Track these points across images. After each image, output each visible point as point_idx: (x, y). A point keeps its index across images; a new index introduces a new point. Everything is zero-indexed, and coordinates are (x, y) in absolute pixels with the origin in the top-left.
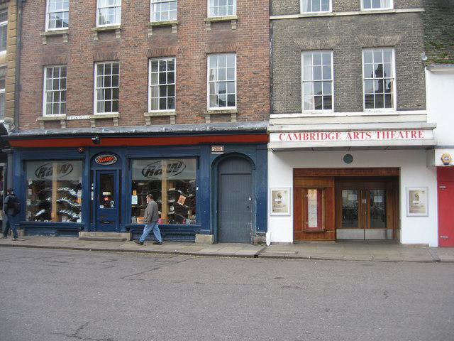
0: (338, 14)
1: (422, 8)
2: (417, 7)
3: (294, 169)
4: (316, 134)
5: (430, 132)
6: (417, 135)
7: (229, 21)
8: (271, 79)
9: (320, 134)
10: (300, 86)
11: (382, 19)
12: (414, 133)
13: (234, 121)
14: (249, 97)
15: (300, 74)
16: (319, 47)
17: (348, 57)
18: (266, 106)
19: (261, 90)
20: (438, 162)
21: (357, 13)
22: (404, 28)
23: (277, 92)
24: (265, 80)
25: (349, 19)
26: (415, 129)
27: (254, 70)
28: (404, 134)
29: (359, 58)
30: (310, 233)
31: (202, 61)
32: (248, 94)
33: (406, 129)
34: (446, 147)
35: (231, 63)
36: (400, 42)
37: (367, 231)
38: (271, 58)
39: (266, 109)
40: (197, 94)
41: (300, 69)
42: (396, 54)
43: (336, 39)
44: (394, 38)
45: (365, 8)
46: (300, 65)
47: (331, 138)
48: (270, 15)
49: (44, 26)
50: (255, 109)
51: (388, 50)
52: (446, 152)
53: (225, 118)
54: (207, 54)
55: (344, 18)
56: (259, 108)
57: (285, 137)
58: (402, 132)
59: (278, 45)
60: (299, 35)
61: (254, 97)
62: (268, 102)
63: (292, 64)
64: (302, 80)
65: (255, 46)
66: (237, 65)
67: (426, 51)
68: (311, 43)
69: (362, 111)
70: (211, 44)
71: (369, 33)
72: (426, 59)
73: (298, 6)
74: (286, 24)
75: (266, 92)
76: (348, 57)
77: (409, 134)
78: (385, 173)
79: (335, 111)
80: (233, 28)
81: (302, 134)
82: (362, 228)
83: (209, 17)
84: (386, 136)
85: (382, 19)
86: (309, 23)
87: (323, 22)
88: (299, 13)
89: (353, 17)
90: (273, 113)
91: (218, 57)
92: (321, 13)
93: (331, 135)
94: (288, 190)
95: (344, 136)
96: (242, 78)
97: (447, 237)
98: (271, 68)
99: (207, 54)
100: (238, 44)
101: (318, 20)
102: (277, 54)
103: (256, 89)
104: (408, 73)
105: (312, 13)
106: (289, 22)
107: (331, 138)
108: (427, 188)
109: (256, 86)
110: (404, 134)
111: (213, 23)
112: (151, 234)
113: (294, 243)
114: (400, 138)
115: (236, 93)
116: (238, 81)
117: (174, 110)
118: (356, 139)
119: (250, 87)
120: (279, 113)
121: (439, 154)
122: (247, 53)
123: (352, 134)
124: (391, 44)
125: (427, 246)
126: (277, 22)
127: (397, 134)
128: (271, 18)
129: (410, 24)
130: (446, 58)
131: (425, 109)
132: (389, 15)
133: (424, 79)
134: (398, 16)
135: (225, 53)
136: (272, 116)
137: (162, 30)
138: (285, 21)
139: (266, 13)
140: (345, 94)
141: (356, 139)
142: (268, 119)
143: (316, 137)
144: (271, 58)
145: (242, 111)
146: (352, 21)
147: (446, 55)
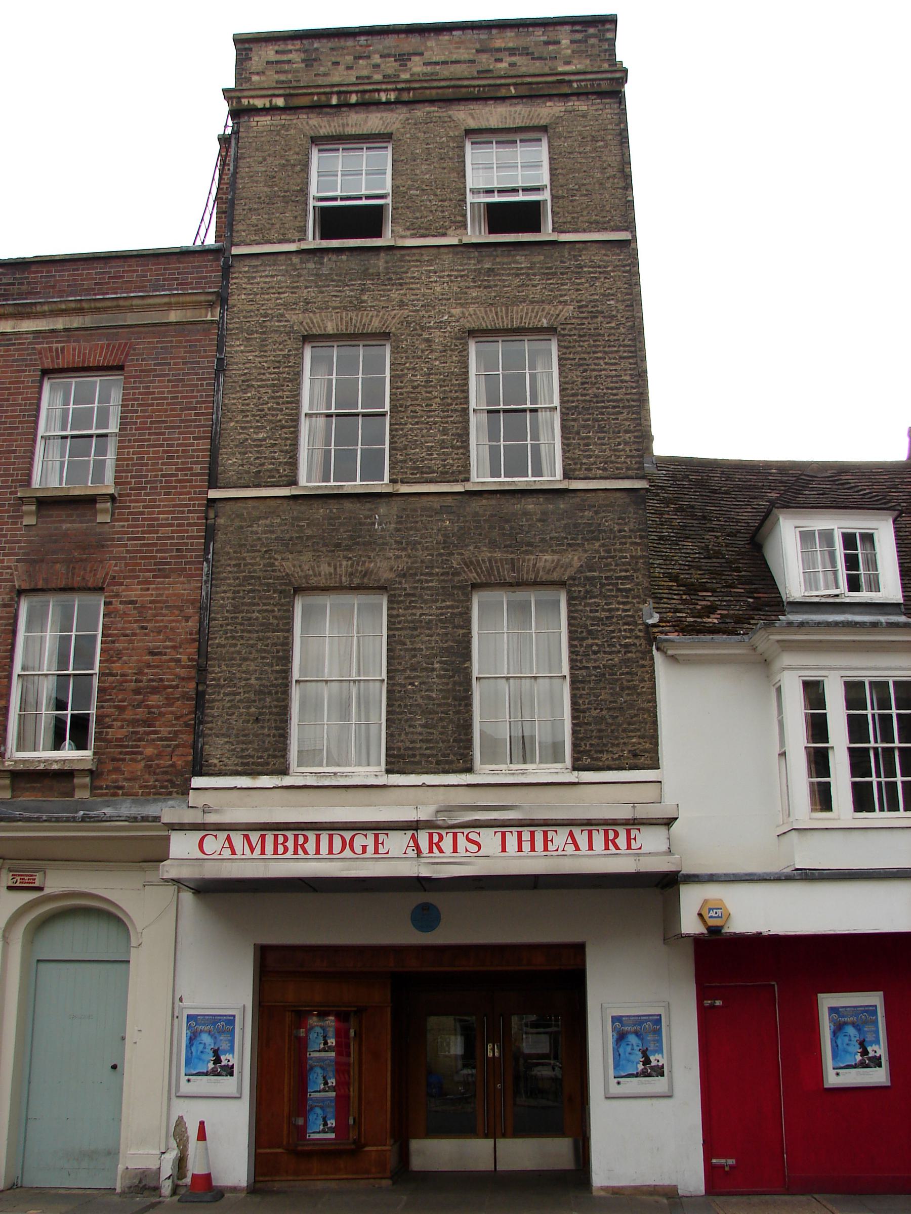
0: (404, 489)
2: (628, 478)
4: (311, 835)
5: (661, 831)
6: (622, 841)
8: (201, 671)
11: (530, 507)
12: (611, 835)
14: (134, 722)
15: (286, 659)
17: (429, 612)
18: (180, 751)
20: (690, 925)
21: (458, 488)
22: (594, 534)
24: (182, 672)
25: (436, 503)
26: (615, 822)
28: (582, 839)
30: (308, 1155)
32: (129, 715)
33: (588, 824)
34: (712, 879)
35: (87, 621)
36: (579, 571)
37: (502, 1143)
38: (204, 609)
42: (569, 605)
44: (565, 560)
49: (36, 423)
50: (150, 759)
51: (547, 594)
52: (712, 892)
54: (21, 592)
56: (159, 756)
57: (214, 844)
58: (576, 831)
60: (289, 545)
61: (147, 723)
62: (187, 738)
63: (266, 627)
64: (296, 675)
67: (658, 599)
68: (325, 569)
70: (33, 561)
71: (493, 545)
72: (655, 619)
73: (293, 464)
74: (255, 513)
75: (184, 708)
80: (100, 519)
82: (486, 1136)
84: (526, 846)
85: (530, 505)
86: (320, 511)
87: (361, 510)
88: (293, 482)
90: (201, 774)
92: (357, 485)
93: (359, 841)
96: (116, 667)
97: (731, 1162)
98: (202, 638)
100: (114, 568)
101: (348, 505)
102: (224, 599)
103: (154, 700)
104: (604, 659)
107: (358, 848)
109: (155, 691)
110: (582, 839)
114: (570, 849)
115: (93, 711)
116: (102, 674)
117: (87, 754)
118: (348, 853)
119: (137, 692)
122: (136, 592)
123: (423, 838)
124: (555, 576)
125: (670, 1194)
127: (560, 838)
128: (213, 494)
130: (713, 620)
133: (653, 678)
136: (197, 782)
140: (420, 720)
142: (185, 790)
143: (311, 846)
144: (204, 609)
147: (711, 610)
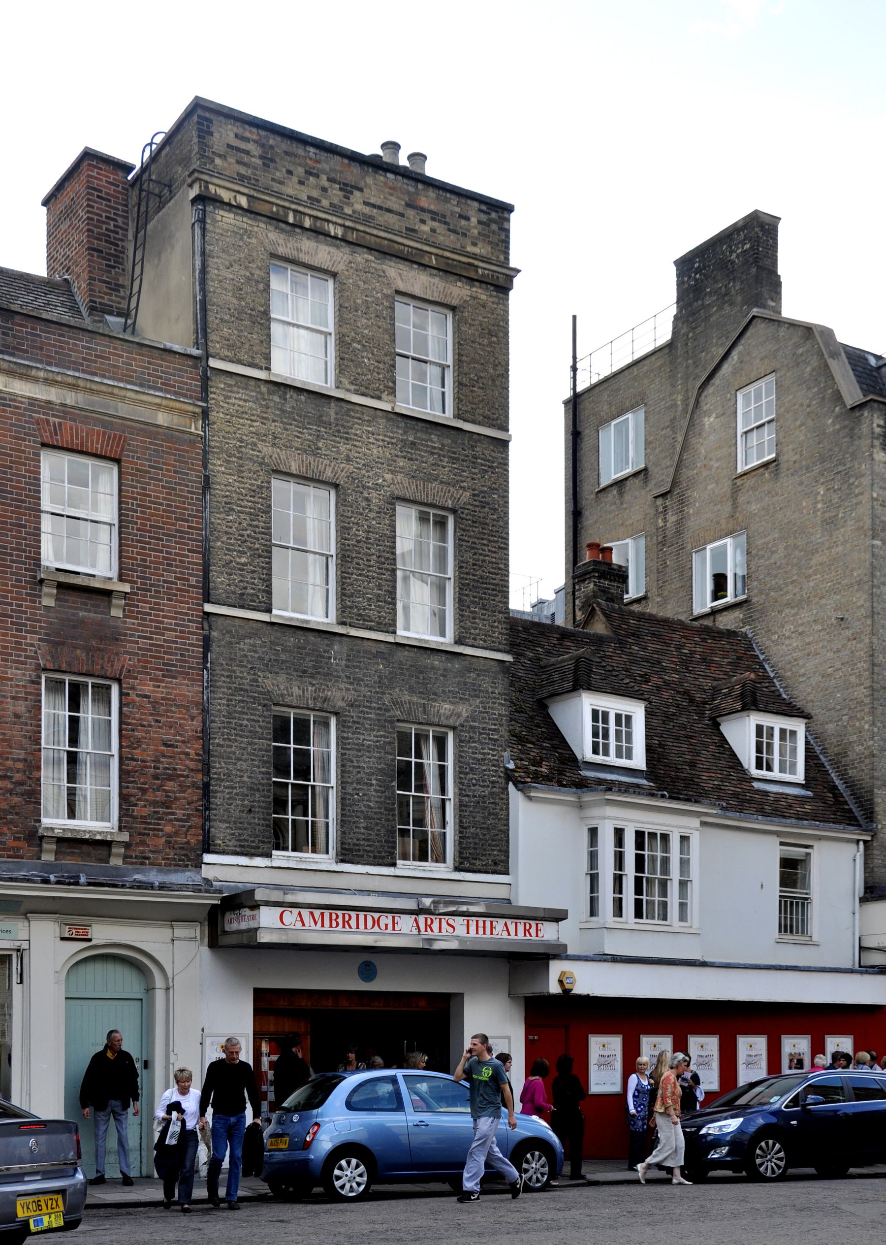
0: (353, 632)
1: (508, 652)
3: (259, 994)
9: (362, 915)
14: (155, 803)
19: (183, 788)
22: (476, 692)
24: (192, 765)
25: (374, 648)
32: (150, 796)
40: (18, 776)
47: (383, 926)
56: (176, 833)
57: (291, 917)
58: (509, 921)
59: (221, 681)
62: (197, 821)
69: (394, 865)
71: (412, 690)
75: (194, 795)
79: (457, 869)
81: (327, 913)
86: (291, 640)
88: (269, 610)
89: (382, 646)
94: (786, 1071)
98: (205, 735)
100: (128, 662)
101: (311, 637)
102: (219, 706)
103: (170, 785)
104: (479, 791)
107: (383, 926)
108: (509, 1038)
109: (170, 778)
112: (351, 1187)
118: (376, 929)
119: (156, 777)
121: (556, 968)
122: (148, 688)
128: (209, 608)
131: (506, 873)
132: (422, 651)
136: (208, 858)
139: (197, 593)
140: (363, 823)
141: (376, 929)
143: (353, 923)
146: (379, 655)
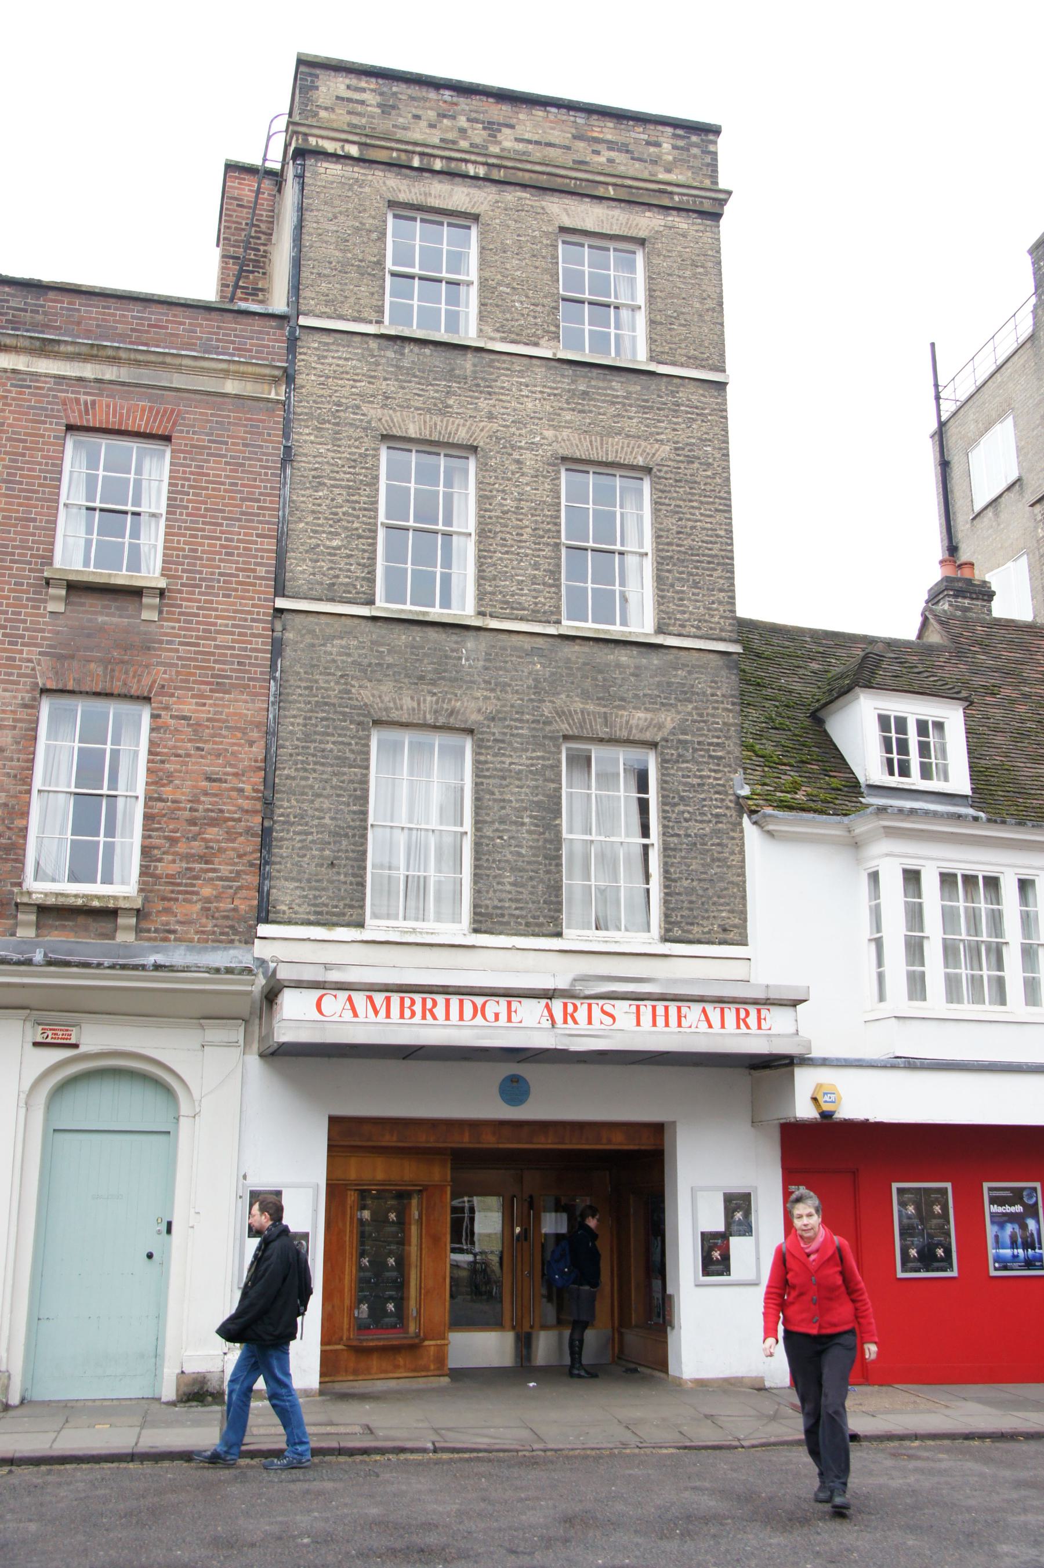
0: (494, 624)
3: (333, 1121)
4: (441, 999)
5: (788, 1012)
6: (752, 1020)
7: (136, 592)
10: (364, 836)
11: (624, 659)
12: (742, 1014)
13: (126, 937)
14: (188, 857)
15: (364, 799)
16: (430, 719)
17: (520, 761)
18: (244, 893)
21: (551, 630)
22: (686, 694)
23: (284, 850)
24: (247, 804)
25: (527, 643)
27: (215, 768)
29: (552, 767)
31: (22, 713)
32: (181, 848)
38: (271, 734)
39: (246, 903)
41: (364, 781)
43: (486, 698)
45: (568, 619)
46: (367, 768)
47: (490, 1016)
48: (276, 595)
50: (208, 900)
53: (95, 925)
54: (44, 691)
55: (515, 638)
56: (218, 898)
58: (709, 1008)
59: (297, 694)
60: (369, 672)
61: (204, 859)
62: (252, 879)
63: (342, 761)
65: (221, 688)
66: (152, 743)
68: (408, 703)
70: (61, 656)
71: (586, 696)
74: (329, 631)
75: (249, 845)
76: (520, 761)
77: (730, 1016)
78: (618, 1142)
80: (146, 615)
81: (395, 998)
83: (58, 563)
84: (661, 1021)
85: (624, 657)
86: (402, 637)
88: (371, 602)
90: (267, 921)
91: (80, 706)
95: (530, 1012)
96: (167, 791)
98: (269, 766)
99: (44, 691)
100: (161, 674)
101: (432, 634)
102: (293, 725)
104: (695, 828)
105: (408, 609)
106: (338, 624)
107: (490, 1016)
109: (213, 823)
111: (76, 588)
113: (322, 1392)
114: (703, 1026)
119: (192, 822)
120: (289, 922)
121: (805, 1081)
122: (188, 707)
123: (557, 1005)
124: (648, 736)
126: (299, 619)
128: (281, 603)
129: (702, 683)
133: (742, 852)
134: (671, 656)
135: (108, 695)
136: (263, 930)
137: (419, 628)
138: (323, 620)
139: (267, 587)
140: (509, 877)
142: (250, 939)
143: (440, 1011)
144: (271, 734)
145: (160, 905)
